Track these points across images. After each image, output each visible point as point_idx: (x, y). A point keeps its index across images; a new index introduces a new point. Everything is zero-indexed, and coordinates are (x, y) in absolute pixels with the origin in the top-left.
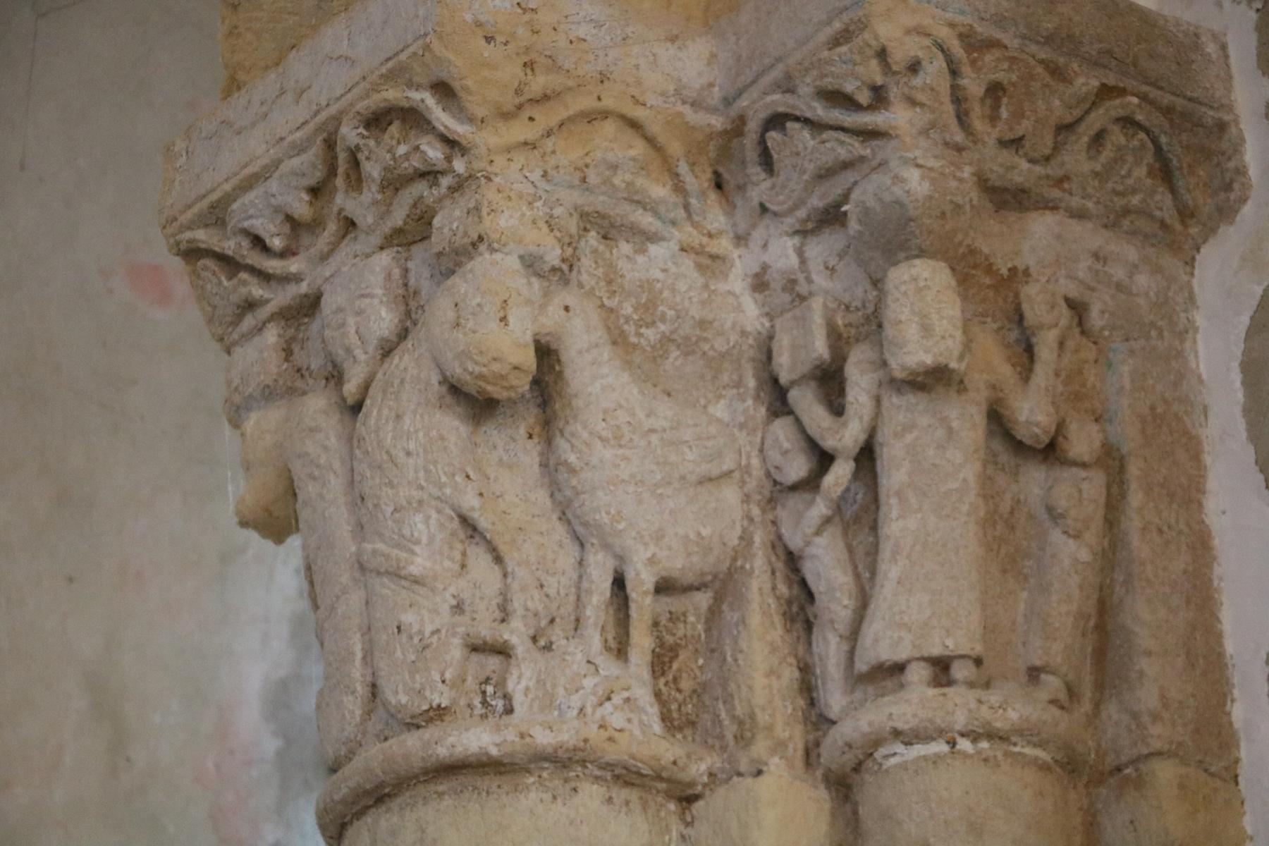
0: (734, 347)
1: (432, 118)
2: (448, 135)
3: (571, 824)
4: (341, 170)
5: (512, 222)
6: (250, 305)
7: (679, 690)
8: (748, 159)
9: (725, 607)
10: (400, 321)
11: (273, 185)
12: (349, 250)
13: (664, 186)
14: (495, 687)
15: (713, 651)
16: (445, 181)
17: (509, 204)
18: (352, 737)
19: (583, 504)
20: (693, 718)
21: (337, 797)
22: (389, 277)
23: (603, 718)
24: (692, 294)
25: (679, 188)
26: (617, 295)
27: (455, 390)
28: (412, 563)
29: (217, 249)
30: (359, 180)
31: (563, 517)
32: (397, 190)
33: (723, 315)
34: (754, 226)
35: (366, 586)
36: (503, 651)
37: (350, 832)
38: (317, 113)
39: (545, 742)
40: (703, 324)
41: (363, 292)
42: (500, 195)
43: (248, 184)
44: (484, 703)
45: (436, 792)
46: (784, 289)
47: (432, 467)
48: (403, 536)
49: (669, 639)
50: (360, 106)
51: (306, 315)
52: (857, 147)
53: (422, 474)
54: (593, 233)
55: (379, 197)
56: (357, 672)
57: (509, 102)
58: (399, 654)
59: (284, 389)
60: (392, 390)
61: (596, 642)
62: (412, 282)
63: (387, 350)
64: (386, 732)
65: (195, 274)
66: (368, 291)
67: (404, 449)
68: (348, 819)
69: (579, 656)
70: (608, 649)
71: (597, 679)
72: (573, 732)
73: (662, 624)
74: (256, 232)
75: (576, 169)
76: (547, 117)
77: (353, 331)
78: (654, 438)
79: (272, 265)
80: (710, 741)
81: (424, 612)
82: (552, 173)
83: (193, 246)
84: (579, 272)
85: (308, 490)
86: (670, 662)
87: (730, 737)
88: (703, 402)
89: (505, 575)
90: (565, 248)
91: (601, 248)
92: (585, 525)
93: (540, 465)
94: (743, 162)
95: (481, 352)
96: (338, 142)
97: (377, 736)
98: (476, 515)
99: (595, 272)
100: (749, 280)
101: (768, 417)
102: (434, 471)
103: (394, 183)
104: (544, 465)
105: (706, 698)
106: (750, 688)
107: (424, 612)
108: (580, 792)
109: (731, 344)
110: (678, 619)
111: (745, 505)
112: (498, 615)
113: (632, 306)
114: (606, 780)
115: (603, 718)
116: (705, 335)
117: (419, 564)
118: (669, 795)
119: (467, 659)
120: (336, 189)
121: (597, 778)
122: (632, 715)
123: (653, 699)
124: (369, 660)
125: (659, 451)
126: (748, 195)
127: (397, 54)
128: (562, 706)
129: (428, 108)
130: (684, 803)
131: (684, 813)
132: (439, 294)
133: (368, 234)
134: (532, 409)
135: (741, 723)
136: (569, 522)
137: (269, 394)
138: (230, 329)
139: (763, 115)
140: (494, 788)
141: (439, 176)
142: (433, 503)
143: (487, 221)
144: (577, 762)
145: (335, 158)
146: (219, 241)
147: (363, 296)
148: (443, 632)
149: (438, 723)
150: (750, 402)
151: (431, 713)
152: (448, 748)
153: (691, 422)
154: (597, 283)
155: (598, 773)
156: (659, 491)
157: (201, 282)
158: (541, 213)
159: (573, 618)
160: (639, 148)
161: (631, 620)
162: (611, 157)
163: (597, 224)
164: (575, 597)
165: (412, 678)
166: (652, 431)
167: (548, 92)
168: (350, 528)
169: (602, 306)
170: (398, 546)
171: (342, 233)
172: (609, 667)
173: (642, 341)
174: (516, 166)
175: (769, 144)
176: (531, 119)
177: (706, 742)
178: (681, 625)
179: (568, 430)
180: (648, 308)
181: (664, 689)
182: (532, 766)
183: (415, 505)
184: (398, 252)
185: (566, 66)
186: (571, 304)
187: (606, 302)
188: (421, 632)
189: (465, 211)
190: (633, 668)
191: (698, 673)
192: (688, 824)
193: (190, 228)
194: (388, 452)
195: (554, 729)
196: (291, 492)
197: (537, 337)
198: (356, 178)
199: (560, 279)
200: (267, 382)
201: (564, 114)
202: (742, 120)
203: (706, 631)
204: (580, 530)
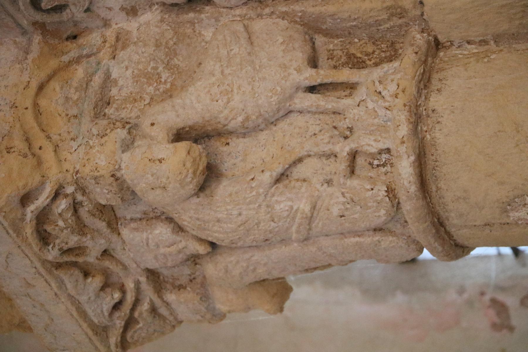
0: (171, 26)
1: (42, 206)
2: (52, 197)
3: (453, 112)
4: (74, 259)
5: (102, 157)
6: (153, 310)
7: (374, 52)
8: (58, 20)
9: (324, 27)
10: (162, 221)
11: (83, 299)
12: (120, 253)
13: (76, 70)
14: (374, 159)
15: (350, 33)
16: (79, 197)
17: (92, 159)
18: (404, 241)
19: (266, 112)
20: (389, 44)
21: (440, 249)
22: (136, 229)
23: (391, 96)
24: (140, 52)
25: (78, 60)
26: (143, 96)
27: (202, 188)
28: (303, 210)
29: (121, 330)
30: (79, 248)
31: (274, 123)
32: (85, 226)
33: (152, 33)
34: (99, 16)
35: (317, 237)
36: (354, 155)
37: (460, 241)
38: (40, 274)
39: (406, 129)
40: (158, 45)
41: (145, 244)
42: (87, 165)
43: (83, 314)
44: (384, 165)
45: (437, 192)
47: (248, 200)
48: (288, 216)
49: (344, 59)
50: (36, 249)
51: (159, 277)
53: (251, 206)
54: (106, 111)
55: (89, 236)
56: (367, 240)
57: (31, 161)
58: (356, 216)
59: (202, 289)
60: (203, 225)
61: (348, 101)
62: (139, 216)
63: (179, 229)
64: (402, 222)
65: (135, 343)
66: (144, 241)
67: (237, 217)
68: (452, 242)
69: (355, 111)
70: (350, 95)
71: (369, 100)
72: (400, 113)
73: (335, 64)
74: (111, 308)
75: (69, 121)
76: (39, 140)
77: (168, 250)
78: (227, 71)
79: (130, 298)
80: (403, 33)
81: (332, 202)
82: (72, 135)
83: (119, 344)
84: (130, 118)
85: (262, 273)
86: (357, 58)
87: (400, 21)
88: (203, 44)
89: (309, 156)
90: (116, 126)
91: (115, 105)
92: (278, 110)
93: (244, 137)
94: (60, 22)
95: (180, 173)
96: (58, 261)
97: (404, 227)
98: (274, 174)
99: (130, 109)
100: (130, 18)
101: (211, 5)
102: (250, 199)
104: (244, 135)
105: (377, 36)
106: (371, 10)
107: (332, 202)
108: (436, 107)
109: (169, 28)
110: (332, 55)
111: (264, 17)
112: (332, 159)
113: (149, 87)
114: (427, 93)
115: (391, 96)
116: (164, 44)
117: (304, 206)
118: (435, 56)
119: (359, 176)
120: (85, 262)
121: (426, 98)
122: (389, 79)
123: (380, 67)
124: (360, 234)
125: (234, 68)
126: (79, 20)
127: (5, 228)
128: (385, 120)
129: (37, 209)
130: (439, 47)
131: (445, 47)
132: (146, 199)
133: (111, 242)
134: (212, 144)
135: (392, 15)
136: (277, 120)
138: (168, 321)
139: (32, 11)
140: (434, 158)
141: (76, 201)
142: (268, 199)
143: (102, 172)
144: (417, 110)
145: (66, 263)
146: (116, 329)
147: (147, 244)
148: (343, 190)
149: (396, 191)
150: (203, 16)
151: (391, 196)
152: (411, 185)
153: (216, 50)
154: (136, 107)
155: (423, 98)
156: (258, 68)
157: (141, 340)
158: (97, 141)
159: (333, 116)
160: (55, 85)
161: (333, 82)
162: (61, 101)
163: (101, 108)
164: (321, 115)
166: (222, 72)
167: (24, 138)
168: (284, 247)
169: (149, 104)
170: (294, 218)
171: (111, 257)
172: (361, 93)
173: (169, 80)
174: (69, 157)
175: (49, 7)
176: (40, 148)
177: (403, 35)
178: (335, 53)
179: (223, 121)
180: (150, 77)
181: (373, 61)
182: (420, 136)
183: (270, 210)
184: (121, 224)
185: (8, 128)
186: (150, 122)
187: (147, 101)
188: (344, 203)
189: (97, 185)
190: (362, 80)
191: (363, 41)
192: (452, 44)
193: (109, 347)
194: (239, 226)
195: (398, 124)
196: (262, 282)
197: (170, 141)
198: (78, 250)
199: (134, 129)
200: (199, 299)
201: (37, 129)
202: (35, 24)
203: (338, 38)
204: (281, 113)
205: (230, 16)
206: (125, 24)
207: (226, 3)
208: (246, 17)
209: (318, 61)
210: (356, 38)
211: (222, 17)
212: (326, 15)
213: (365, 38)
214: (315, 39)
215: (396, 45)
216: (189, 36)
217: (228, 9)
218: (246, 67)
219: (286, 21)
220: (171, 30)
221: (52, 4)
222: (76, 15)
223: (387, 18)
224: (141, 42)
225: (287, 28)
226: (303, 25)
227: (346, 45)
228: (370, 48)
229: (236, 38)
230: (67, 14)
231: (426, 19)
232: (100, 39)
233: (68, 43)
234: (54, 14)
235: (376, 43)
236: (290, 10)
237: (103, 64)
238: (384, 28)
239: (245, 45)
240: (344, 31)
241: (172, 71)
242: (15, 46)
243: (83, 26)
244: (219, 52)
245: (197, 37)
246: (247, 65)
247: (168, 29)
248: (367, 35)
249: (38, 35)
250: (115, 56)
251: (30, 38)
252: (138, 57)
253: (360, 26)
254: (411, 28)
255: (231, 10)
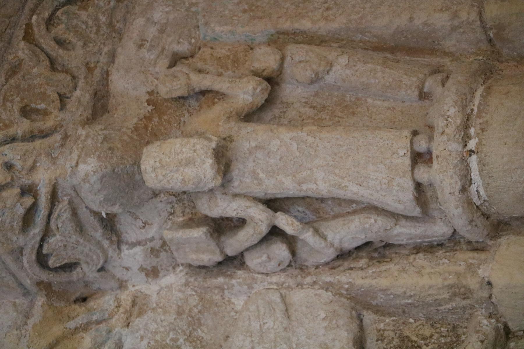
0: (196, 291)
7: (431, 336)
8: (67, 280)
9: (374, 303)
15: (404, 312)
20: (450, 327)
24: (159, 320)
25: (85, 327)
33: (174, 298)
34: (114, 276)
40: (180, 313)
52: (63, 206)
73: (385, 347)
80: (467, 316)
86: (412, 341)
88: (233, 314)
94: (69, 282)
100: (150, 280)
101: (244, 269)
106: (430, 287)
109: (194, 293)
116: (187, 311)
126: (91, 280)
130: (510, 336)
131: (517, 336)
135: (455, 295)
139: (37, 269)
150: (234, 281)
175: (58, 265)
177: (467, 319)
178: (386, 333)
191: (420, 322)
202: (39, 284)
203: (391, 317)
205: (266, 283)
206: (143, 286)
207: (262, 268)
208: (284, 286)
209: (366, 342)
210: (411, 318)
211: (256, 283)
212: (376, 289)
213: (422, 319)
214: (364, 316)
215: (458, 329)
216: (217, 303)
217: (264, 275)
218: (281, 345)
219: (330, 293)
220: (196, 296)
221: (61, 262)
222: (87, 274)
223: (448, 297)
224: (160, 308)
225: (331, 302)
226: (350, 298)
227: (399, 326)
228: (427, 331)
229: (270, 310)
230: (78, 273)
231: (494, 302)
232: (114, 303)
233: (76, 306)
234: (63, 273)
235: (435, 325)
236: (336, 281)
237: (114, 332)
238: (445, 309)
239: (280, 319)
240: (397, 308)
241: (194, 344)
242: (14, 308)
243: (95, 287)
244: (250, 325)
245: (226, 305)
246: (282, 343)
247: (193, 295)
248: (424, 315)
249: (42, 297)
250: (129, 323)
251: (32, 300)
252: (156, 326)
253: (416, 305)
254: (476, 311)
255: (267, 276)
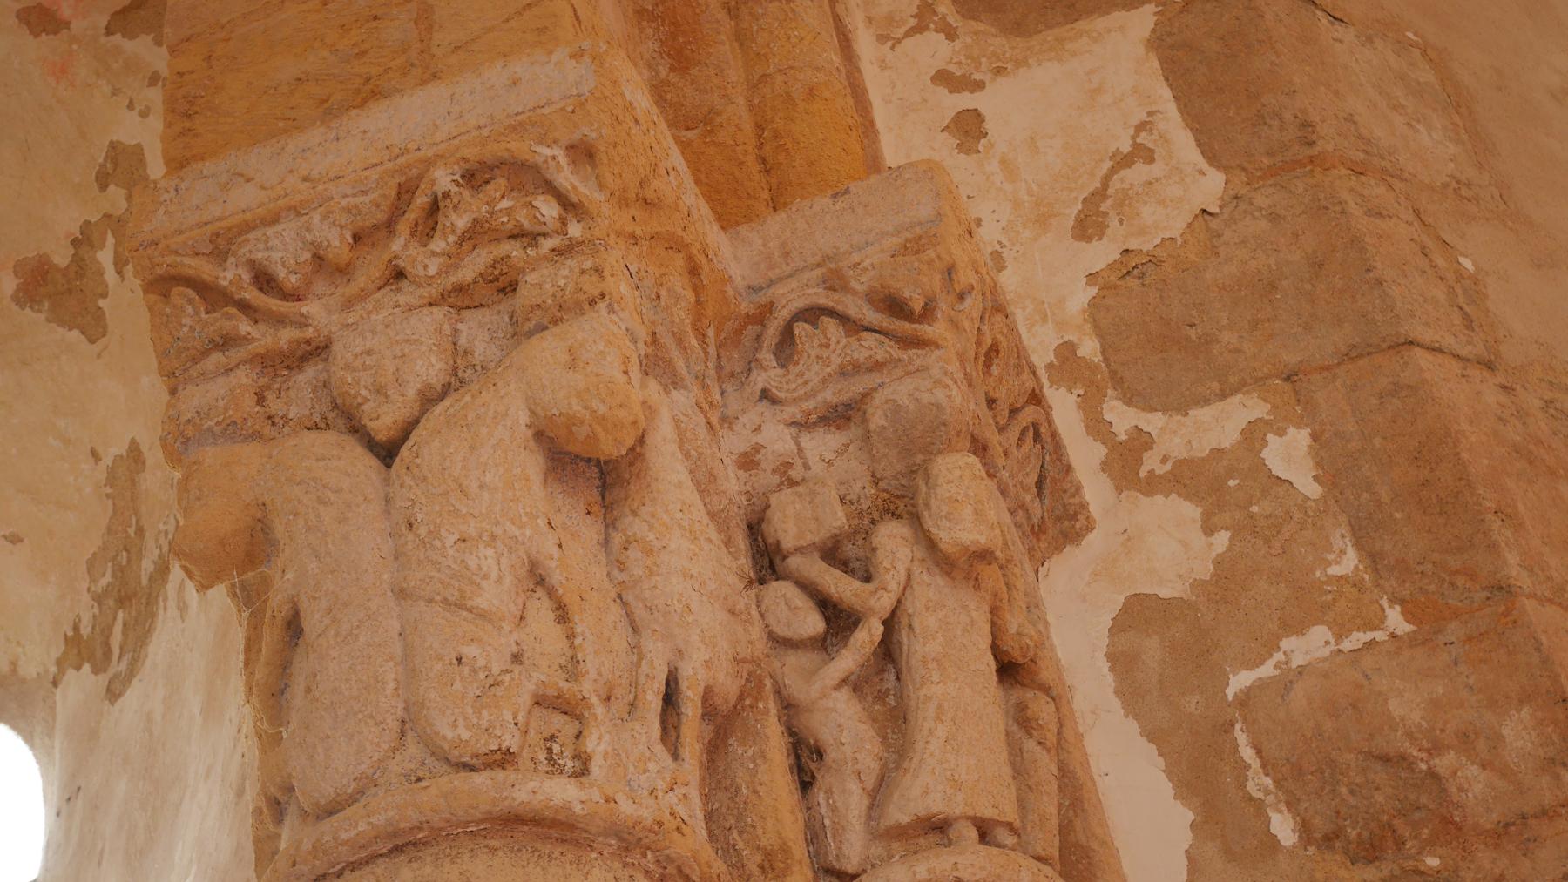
0: (723, 511)
16: (547, 244)
44: (550, 759)
46: (774, 471)
50: (468, 152)
51: (288, 367)
52: (891, 350)
83: (172, 271)
103: (474, 236)
135: (768, 854)
137: (232, 431)
139: (799, 304)
140: (556, 854)
165: (479, 716)
179: (644, 511)
202: (768, 308)
204: (640, 612)
230: (770, 360)
238: (733, 839)
